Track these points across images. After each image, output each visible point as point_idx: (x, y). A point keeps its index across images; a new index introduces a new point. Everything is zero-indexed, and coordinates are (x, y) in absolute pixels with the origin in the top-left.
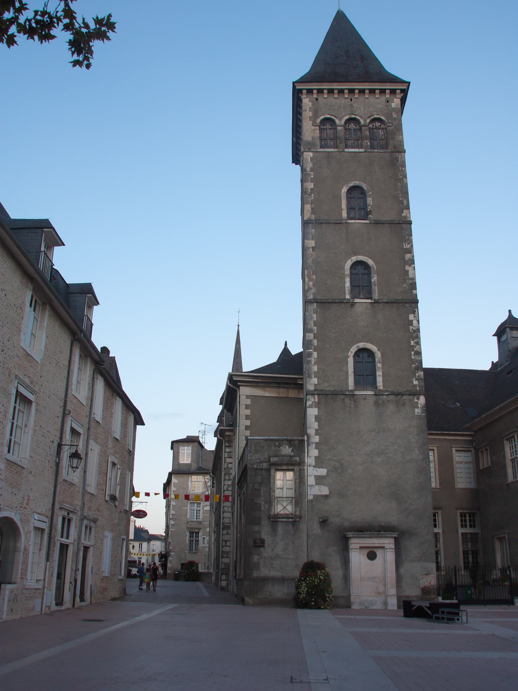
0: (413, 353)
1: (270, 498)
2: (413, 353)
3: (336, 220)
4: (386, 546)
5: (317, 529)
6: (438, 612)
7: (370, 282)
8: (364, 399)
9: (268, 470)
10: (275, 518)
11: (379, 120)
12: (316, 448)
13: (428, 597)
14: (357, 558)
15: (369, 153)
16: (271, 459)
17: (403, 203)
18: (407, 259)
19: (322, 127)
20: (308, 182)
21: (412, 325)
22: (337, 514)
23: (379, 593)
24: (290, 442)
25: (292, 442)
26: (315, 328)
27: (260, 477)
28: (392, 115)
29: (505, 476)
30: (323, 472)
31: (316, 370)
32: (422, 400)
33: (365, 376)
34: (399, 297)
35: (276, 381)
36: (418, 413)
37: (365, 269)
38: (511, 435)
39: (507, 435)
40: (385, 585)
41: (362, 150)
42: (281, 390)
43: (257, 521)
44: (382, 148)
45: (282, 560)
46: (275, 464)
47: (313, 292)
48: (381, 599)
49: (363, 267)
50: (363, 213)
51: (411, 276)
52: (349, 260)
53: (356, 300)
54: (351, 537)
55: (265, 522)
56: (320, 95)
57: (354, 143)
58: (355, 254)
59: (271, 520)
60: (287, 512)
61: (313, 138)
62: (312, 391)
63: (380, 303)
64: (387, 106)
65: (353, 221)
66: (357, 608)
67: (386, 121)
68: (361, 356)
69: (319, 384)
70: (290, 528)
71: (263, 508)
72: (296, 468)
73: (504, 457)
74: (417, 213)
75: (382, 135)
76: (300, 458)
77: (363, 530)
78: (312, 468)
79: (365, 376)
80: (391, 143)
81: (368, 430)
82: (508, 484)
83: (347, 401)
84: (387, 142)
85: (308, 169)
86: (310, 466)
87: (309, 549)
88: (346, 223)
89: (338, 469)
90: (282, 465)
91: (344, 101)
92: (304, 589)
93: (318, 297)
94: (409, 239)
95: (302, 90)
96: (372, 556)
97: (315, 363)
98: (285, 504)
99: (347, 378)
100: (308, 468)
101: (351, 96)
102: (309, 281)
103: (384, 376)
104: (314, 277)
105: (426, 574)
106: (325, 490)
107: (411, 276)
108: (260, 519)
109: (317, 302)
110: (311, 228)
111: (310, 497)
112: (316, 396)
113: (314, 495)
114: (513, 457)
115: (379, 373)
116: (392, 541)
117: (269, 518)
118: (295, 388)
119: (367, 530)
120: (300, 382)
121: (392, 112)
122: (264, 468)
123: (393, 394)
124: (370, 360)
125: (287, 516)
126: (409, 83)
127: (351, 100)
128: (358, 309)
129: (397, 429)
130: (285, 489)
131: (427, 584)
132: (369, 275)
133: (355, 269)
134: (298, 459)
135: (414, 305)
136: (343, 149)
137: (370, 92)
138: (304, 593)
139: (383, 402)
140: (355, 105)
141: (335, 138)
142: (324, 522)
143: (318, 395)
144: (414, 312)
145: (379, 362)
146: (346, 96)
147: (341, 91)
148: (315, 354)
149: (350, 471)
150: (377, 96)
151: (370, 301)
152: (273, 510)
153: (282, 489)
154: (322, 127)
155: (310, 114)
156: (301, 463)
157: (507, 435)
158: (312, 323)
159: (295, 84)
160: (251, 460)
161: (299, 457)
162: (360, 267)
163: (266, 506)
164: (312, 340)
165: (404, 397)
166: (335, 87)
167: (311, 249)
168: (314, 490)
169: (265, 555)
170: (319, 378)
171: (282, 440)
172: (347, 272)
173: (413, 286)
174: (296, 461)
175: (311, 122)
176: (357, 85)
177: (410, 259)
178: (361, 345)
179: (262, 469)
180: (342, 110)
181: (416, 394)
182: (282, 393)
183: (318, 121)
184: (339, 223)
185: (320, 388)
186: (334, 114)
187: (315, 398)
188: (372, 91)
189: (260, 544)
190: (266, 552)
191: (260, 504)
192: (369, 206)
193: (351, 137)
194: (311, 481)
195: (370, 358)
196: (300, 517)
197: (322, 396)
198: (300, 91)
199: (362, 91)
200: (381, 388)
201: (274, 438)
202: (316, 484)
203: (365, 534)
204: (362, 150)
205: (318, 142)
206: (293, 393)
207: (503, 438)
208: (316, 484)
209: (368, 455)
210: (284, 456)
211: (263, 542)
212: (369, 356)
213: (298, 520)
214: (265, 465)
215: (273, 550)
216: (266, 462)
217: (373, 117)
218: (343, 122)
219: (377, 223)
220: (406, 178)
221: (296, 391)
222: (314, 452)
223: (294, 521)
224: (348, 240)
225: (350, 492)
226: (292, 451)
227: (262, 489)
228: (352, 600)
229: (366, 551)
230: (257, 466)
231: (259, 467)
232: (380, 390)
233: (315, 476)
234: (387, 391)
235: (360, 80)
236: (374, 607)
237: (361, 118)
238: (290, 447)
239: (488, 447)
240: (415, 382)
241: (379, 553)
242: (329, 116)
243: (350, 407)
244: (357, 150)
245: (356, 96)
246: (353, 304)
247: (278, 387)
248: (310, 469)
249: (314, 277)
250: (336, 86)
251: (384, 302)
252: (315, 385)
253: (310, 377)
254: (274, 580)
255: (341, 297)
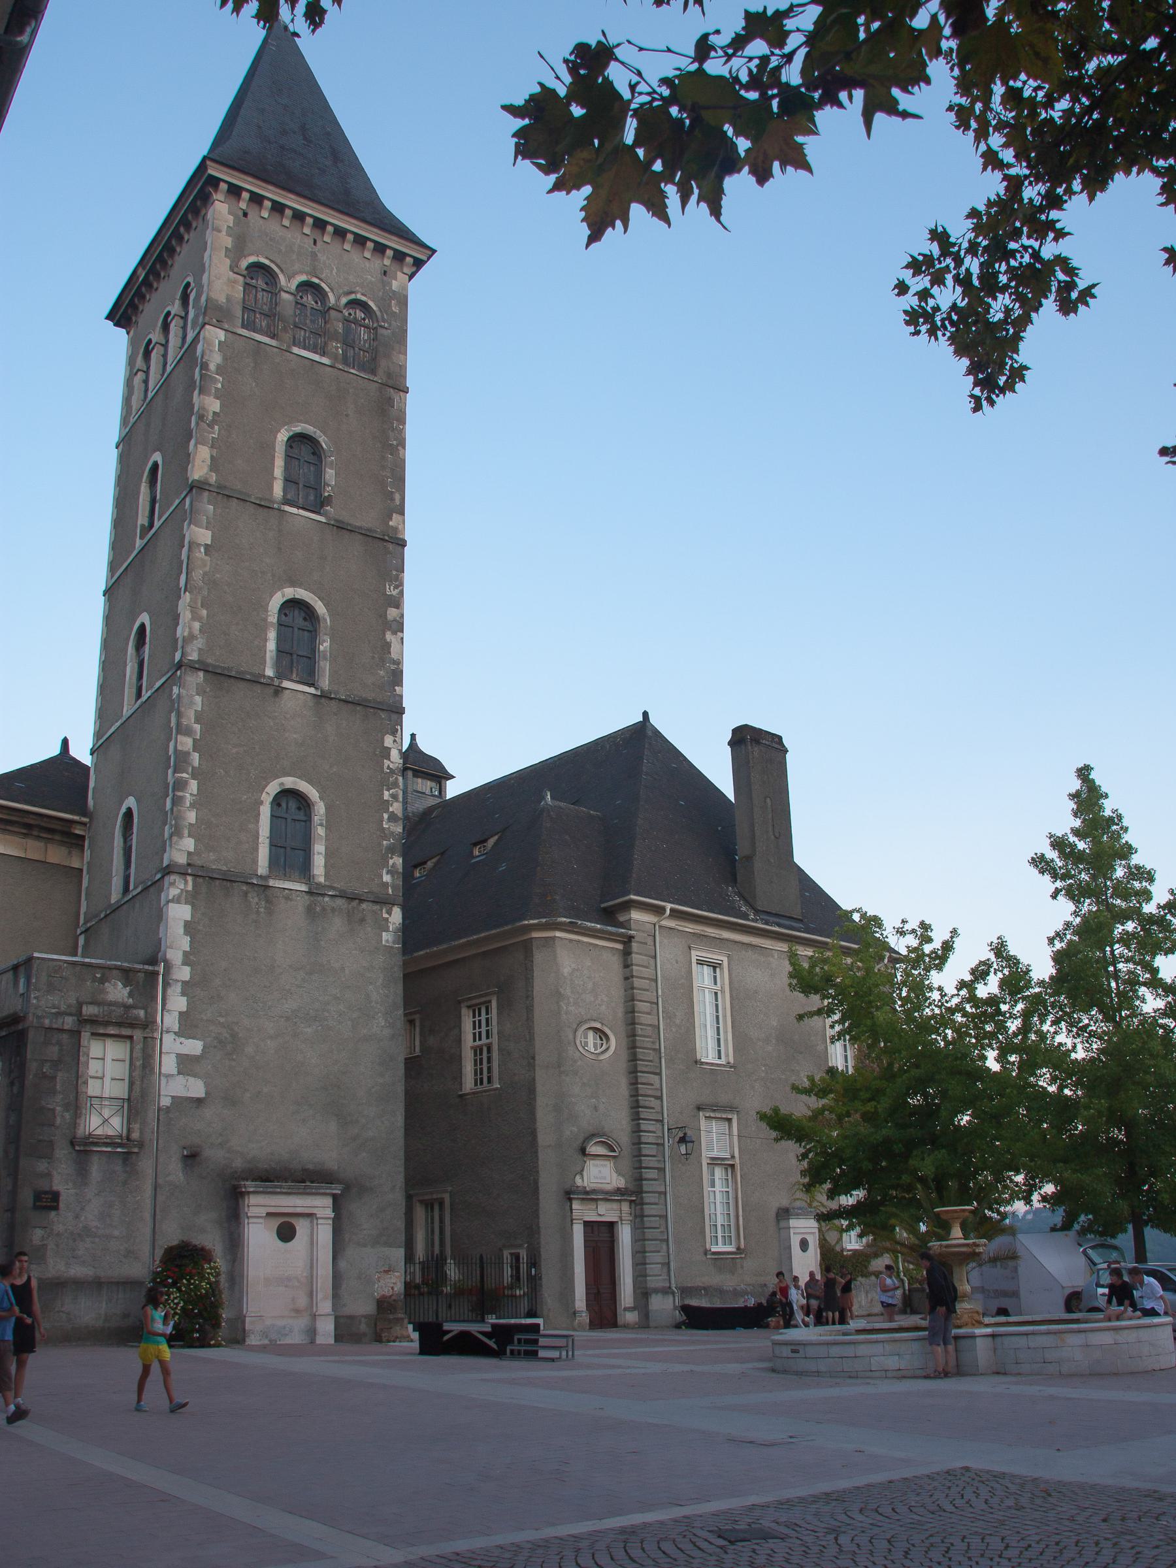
0: (386, 816)
1: (77, 1098)
2: (386, 816)
3: (261, 499)
4: (319, 1213)
5: (175, 1171)
6: (511, 1342)
7: (314, 650)
8: (287, 898)
9: (76, 1034)
10: (86, 1144)
11: (363, 306)
12: (183, 994)
13: (391, 1317)
14: (258, 1236)
15: (340, 373)
16: (84, 1008)
17: (393, 500)
18: (390, 617)
19: (249, 281)
20: (209, 395)
21: (388, 757)
22: (220, 1140)
23: (297, 1311)
24: (127, 975)
25: (131, 974)
26: (197, 727)
27: (56, 1048)
28: (390, 306)
29: (458, 1077)
30: (194, 1047)
31: (193, 821)
32: (396, 917)
33: (291, 852)
34: (370, 695)
35: (26, 820)
36: (387, 941)
37: (305, 619)
38: (483, 999)
39: (470, 999)
40: (311, 1295)
41: (325, 360)
42: (31, 843)
43: (45, 1150)
44: (362, 368)
45: (97, 1240)
46: (93, 1021)
47: (200, 646)
48: (302, 1322)
49: (303, 614)
50: (312, 498)
51: (394, 655)
52: (279, 594)
53: (286, 684)
54: (249, 1193)
55: (62, 1152)
56: (255, 207)
57: (309, 338)
58: (293, 584)
59: (77, 1148)
60: (110, 1132)
61: (228, 299)
62: (181, 866)
63: (331, 699)
64: (384, 284)
65: (294, 510)
66: (258, 1343)
67: (378, 313)
68: (284, 805)
69: (197, 852)
70: (118, 1167)
71: (58, 1121)
72: (138, 1034)
73: (459, 1041)
74: (419, 524)
75: (365, 341)
76: (146, 1012)
77: (273, 1177)
78: (173, 1036)
79: (291, 852)
80: (383, 363)
81: (290, 966)
82: (461, 1096)
83: (253, 899)
84: (374, 359)
85: (212, 367)
86: (168, 1032)
87: (158, 1217)
88: (279, 510)
89: (226, 1044)
90: (107, 1024)
91: (300, 238)
92: (177, 1304)
93: (210, 661)
94: (397, 576)
95: (219, 180)
96: (286, 1233)
97: (192, 806)
98: (106, 1113)
99: (256, 849)
100: (165, 1036)
101: (317, 234)
102: (193, 619)
103: (329, 855)
104: (204, 612)
105: (386, 1272)
106: (196, 1088)
107: (394, 655)
108: (51, 1144)
109: (206, 671)
110: (205, 500)
111: (166, 1102)
112: (189, 879)
113: (173, 1097)
114: (478, 1043)
115: (319, 848)
116: (328, 1201)
117: (72, 1144)
118: (62, 843)
119: (278, 1179)
120: (77, 832)
121: (391, 298)
122: (66, 1027)
123: (343, 895)
124: (301, 816)
125: (109, 1141)
126: (434, 251)
127: (315, 242)
128: (288, 703)
129: (347, 972)
130: (107, 1080)
131: (387, 1292)
132: (313, 633)
133: (286, 615)
134: (142, 1013)
135: (394, 716)
136: (289, 347)
137: (375, 250)
138: (176, 1313)
139: (324, 909)
140: (322, 258)
141: (271, 315)
142: (191, 1158)
143: (195, 876)
144: (394, 732)
145: (321, 825)
146: (307, 230)
147: (299, 217)
148: (193, 786)
149: (249, 1050)
150: (367, 254)
151: (312, 690)
152: (82, 1125)
153: (102, 1078)
154: (249, 281)
155: (228, 242)
156: (148, 1024)
157: (470, 999)
158: (191, 714)
159: (208, 163)
160: (37, 1007)
161: (145, 1008)
162: (296, 612)
163: (67, 1115)
164: (188, 753)
165: (364, 906)
166: (289, 203)
167: (202, 550)
168: (175, 1086)
169: (59, 1228)
170: (198, 841)
171: (110, 968)
172: (273, 618)
173: (397, 677)
174: (137, 1018)
175: (228, 262)
176: (390, 240)
177: (395, 620)
178: (289, 782)
179: (61, 1030)
180: (294, 257)
181: (384, 902)
182: (32, 849)
183: (244, 264)
184: (264, 506)
185: (199, 863)
186: (278, 261)
187: (186, 882)
188: (360, 241)
189: (49, 1201)
190: (62, 1221)
191: (53, 1110)
192: (329, 485)
193: (306, 324)
194: (169, 1064)
195: (302, 813)
196: (141, 1145)
197: (201, 880)
198: (214, 182)
199: (340, 233)
200: (322, 880)
201: (93, 961)
202: (179, 1073)
203: (281, 1187)
204: (325, 360)
205: (238, 312)
206: (56, 855)
207: (459, 1002)
208: (179, 1073)
209: (288, 1019)
210: (111, 1004)
211: (56, 1196)
212: (299, 809)
213: (136, 1150)
214: (69, 1022)
215: (77, 1217)
216: (71, 1014)
217: (353, 296)
218: (293, 285)
219: (340, 527)
220: (404, 448)
221: (63, 850)
222: (179, 1002)
223: (126, 1151)
224: (279, 549)
225: (248, 1095)
226: (131, 995)
227: (60, 1076)
228: (247, 1327)
229: (275, 1223)
230: (51, 1021)
231: (55, 1026)
232: (319, 884)
233: (179, 1056)
234: (332, 888)
235: (336, 206)
236: (288, 1340)
237: (332, 289)
238: (125, 986)
239: (417, 1017)
240: (387, 878)
241: (302, 1227)
242: (267, 262)
243: (258, 912)
244: (316, 357)
245: (327, 238)
246: (279, 691)
247: (25, 835)
248: (168, 1039)
249: (204, 612)
250: (292, 202)
251: (340, 700)
252: (189, 853)
253: (177, 832)
254: (79, 1284)
255: (256, 670)
